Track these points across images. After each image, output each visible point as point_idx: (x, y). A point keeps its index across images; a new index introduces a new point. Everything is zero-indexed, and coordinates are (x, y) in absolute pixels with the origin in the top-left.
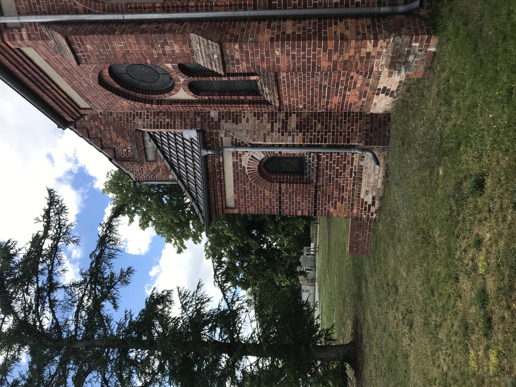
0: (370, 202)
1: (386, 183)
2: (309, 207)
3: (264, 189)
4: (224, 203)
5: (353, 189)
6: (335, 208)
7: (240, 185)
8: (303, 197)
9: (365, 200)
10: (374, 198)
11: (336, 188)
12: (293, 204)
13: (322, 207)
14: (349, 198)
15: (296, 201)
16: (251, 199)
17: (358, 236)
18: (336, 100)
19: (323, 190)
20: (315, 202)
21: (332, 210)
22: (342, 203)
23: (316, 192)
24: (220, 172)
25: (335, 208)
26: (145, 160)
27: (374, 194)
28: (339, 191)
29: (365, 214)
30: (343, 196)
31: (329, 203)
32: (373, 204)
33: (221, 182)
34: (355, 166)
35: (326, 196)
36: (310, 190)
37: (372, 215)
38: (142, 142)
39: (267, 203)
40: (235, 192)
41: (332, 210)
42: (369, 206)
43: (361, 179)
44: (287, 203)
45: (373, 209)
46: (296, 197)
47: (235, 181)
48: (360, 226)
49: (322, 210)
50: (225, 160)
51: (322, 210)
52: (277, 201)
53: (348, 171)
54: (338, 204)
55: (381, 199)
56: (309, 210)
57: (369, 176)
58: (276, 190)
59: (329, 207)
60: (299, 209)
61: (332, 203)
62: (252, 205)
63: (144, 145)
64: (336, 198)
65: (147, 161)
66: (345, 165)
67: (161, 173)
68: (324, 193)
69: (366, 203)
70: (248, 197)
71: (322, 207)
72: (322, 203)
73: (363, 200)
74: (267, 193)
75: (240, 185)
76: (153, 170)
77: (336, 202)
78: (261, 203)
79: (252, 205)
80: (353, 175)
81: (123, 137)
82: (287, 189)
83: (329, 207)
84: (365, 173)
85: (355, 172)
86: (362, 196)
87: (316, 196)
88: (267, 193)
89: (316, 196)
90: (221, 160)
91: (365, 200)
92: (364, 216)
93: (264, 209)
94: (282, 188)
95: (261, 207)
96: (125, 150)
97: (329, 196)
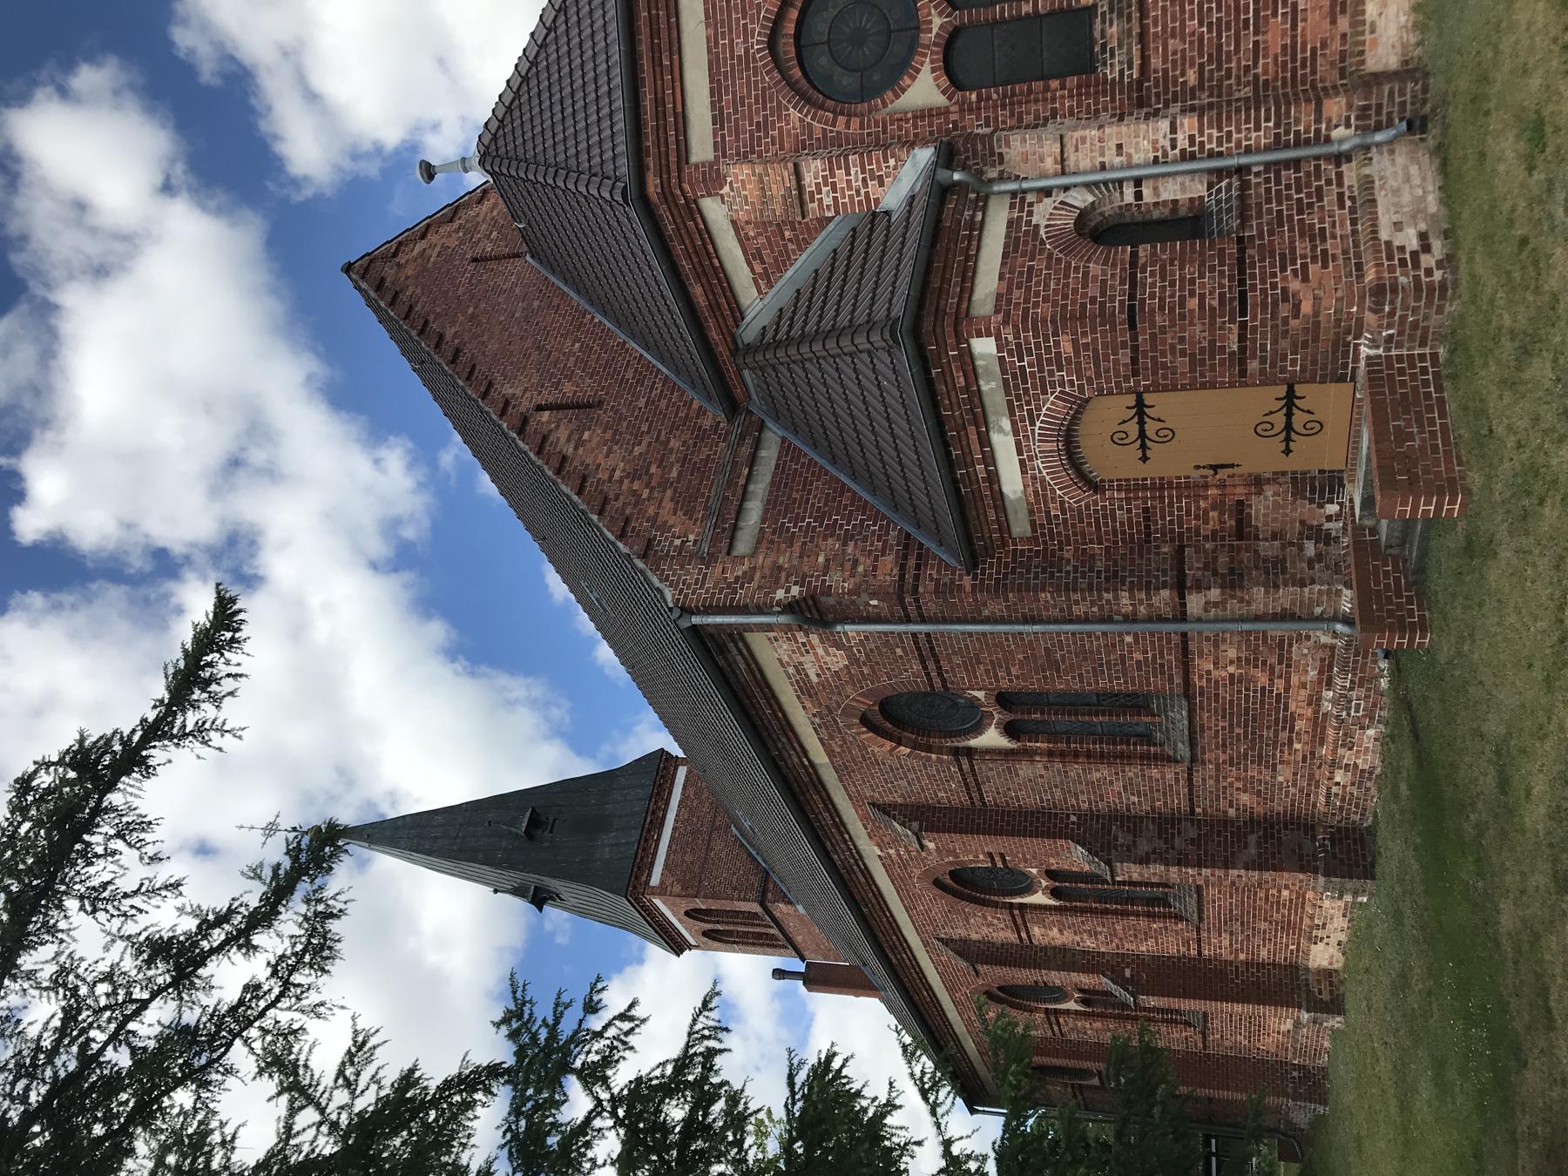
0: (1414, 244)
1: (1448, 195)
2: (1221, 286)
3: (1088, 261)
4: (964, 305)
5: (1355, 232)
6: (1305, 279)
7: (1020, 260)
8: (1202, 265)
9: (1396, 243)
10: (1423, 236)
11: (1302, 235)
12: (1172, 284)
13: (1263, 282)
14: (1345, 252)
15: (1182, 279)
16: (1047, 286)
17: (1403, 436)
18: (1275, 36)
19: (1261, 246)
20: (1242, 272)
21: (1295, 285)
22: (1325, 266)
23: (1242, 251)
24: (970, 237)
25: (1305, 279)
26: (725, 551)
27: (1423, 227)
28: (1312, 239)
29: (1406, 274)
30: (1324, 252)
31: (1283, 269)
32: (1426, 248)
33: (967, 260)
34: (1350, 187)
35: (1272, 256)
36: (1222, 250)
37: (1429, 272)
38: (734, 509)
39: (1094, 290)
40: (1001, 277)
41: (1295, 285)
42: (1414, 254)
43: (1374, 201)
44: (1153, 285)
45: (1427, 260)
46: (1182, 268)
47: (1005, 255)
48: (1404, 404)
49: (1264, 291)
50: (988, 219)
51: (1264, 291)
52: (1122, 283)
53: (1330, 199)
54: (1313, 269)
55: (1447, 234)
56: (1222, 295)
57: (1396, 192)
58: (1122, 261)
59: (1285, 279)
60: (1192, 293)
61: (1295, 272)
62: (1046, 299)
63: (737, 518)
64: (1303, 257)
65: (728, 554)
66: (1319, 189)
67: (754, 584)
68: (1267, 252)
69: (1402, 249)
70: (1038, 284)
71: (1263, 282)
72: (1263, 273)
73: (1388, 244)
74: (1095, 268)
75: (1020, 260)
76: (737, 578)
77: (1304, 266)
78: (1075, 291)
79: (1046, 299)
80: (1348, 203)
81: (689, 513)
82: (1154, 254)
83: (1285, 279)
84: (1382, 187)
85: (1352, 198)
86: (1384, 235)
87: (1241, 261)
88: (1095, 268)
89: (1241, 261)
90: (979, 217)
91: (1396, 243)
92: (1403, 280)
93: (1083, 305)
94: (1141, 254)
95: (1074, 302)
96: (677, 542)
97: (1282, 256)
